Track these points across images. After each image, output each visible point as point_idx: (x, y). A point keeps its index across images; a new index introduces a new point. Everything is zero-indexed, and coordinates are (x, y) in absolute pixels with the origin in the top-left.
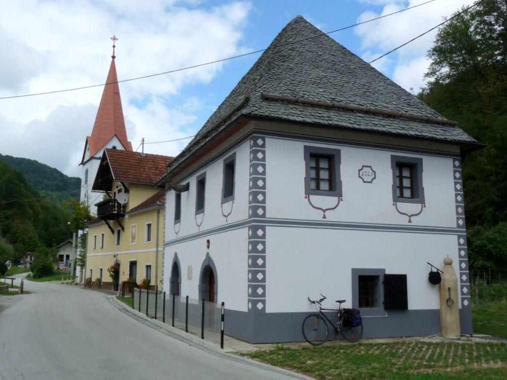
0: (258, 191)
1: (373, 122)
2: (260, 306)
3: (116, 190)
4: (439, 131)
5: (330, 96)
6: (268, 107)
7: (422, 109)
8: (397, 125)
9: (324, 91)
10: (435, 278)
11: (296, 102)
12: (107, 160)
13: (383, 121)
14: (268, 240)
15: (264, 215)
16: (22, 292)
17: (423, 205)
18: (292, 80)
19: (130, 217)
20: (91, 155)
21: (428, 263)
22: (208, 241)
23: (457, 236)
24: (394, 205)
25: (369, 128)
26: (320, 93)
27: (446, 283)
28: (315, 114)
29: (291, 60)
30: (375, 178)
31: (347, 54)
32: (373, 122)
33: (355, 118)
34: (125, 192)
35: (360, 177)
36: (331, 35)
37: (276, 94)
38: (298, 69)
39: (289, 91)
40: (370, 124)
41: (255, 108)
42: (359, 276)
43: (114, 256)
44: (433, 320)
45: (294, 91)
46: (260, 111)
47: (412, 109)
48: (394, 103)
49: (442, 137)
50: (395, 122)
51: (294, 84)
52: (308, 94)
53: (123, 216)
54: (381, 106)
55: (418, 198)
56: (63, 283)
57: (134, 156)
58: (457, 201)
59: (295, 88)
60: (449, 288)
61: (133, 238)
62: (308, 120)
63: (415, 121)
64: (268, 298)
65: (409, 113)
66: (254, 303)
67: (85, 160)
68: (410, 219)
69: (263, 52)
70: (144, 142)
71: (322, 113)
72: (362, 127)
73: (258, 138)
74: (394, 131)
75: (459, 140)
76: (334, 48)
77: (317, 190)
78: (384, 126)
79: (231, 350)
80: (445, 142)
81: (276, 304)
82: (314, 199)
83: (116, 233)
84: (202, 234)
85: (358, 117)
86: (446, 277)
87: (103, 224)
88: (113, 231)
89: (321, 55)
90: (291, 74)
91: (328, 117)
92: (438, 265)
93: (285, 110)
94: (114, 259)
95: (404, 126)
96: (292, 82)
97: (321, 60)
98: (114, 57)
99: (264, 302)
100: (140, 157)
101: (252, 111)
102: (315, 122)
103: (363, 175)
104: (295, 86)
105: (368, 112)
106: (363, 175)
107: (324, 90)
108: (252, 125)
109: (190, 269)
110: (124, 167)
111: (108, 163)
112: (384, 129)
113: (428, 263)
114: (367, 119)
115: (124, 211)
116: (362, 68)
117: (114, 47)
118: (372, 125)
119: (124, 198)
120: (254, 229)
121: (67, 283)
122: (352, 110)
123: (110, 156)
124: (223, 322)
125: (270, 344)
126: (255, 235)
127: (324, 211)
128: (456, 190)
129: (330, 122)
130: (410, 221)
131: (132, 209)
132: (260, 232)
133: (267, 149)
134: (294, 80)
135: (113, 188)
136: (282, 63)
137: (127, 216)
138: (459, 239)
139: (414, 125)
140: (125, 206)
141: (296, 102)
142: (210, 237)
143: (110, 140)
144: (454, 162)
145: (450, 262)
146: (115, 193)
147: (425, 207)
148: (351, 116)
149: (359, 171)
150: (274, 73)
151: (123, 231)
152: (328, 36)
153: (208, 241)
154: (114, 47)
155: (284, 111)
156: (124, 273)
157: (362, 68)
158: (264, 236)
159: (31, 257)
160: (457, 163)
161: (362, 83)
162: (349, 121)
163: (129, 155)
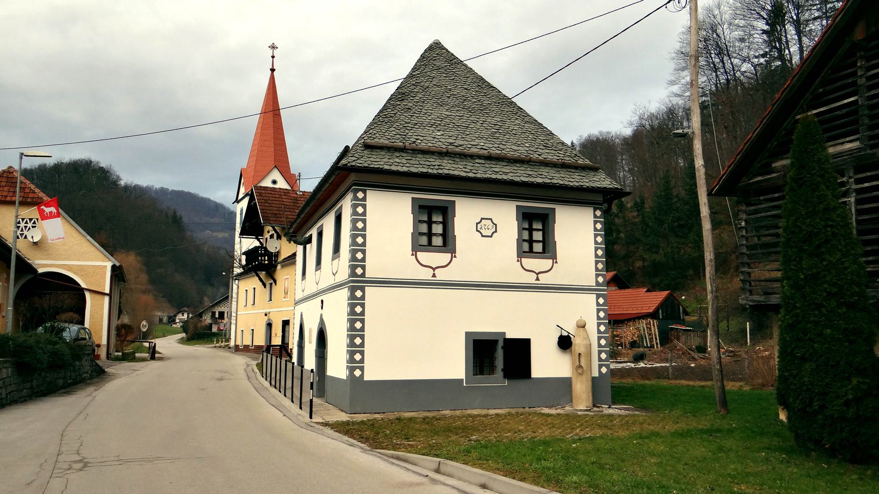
0: (359, 248)
1: (493, 169)
2: (357, 373)
3: (267, 236)
4: (575, 176)
5: (447, 141)
6: (370, 156)
7: (561, 150)
8: (523, 172)
9: (442, 135)
10: (565, 343)
11: (403, 150)
12: (255, 200)
13: (506, 167)
14: (367, 302)
15: (363, 275)
16: (153, 358)
17: (555, 260)
18: (406, 123)
19: (283, 267)
20: (245, 191)
21: (558, 326)
22: (322, 301)
23: (595, 295)
24: (518, 261)
25: (487, 176)
26: (437, 137)
27: (577, 348)
28: (424, 163)
29: (411, 98)
30: (496, 231)
31: (484, 86)
32: (493, 169)
33: (473, 165)
34: (277, 239)
35: (496, 225)
36: (470, 64)
37: (384, 141)
38: (417, 108)
39: (399, 137)
40: (489, 172)
41: (354, 158)
42: (474, 341)
43: (266, 315)
44: (562, 387)
45: (405, 135)
46: (359, 161)
47: (548, 151)
48: (526, 145)
49: (577, 184)
50: (522, 168)
51: (408, 128)
52: (422, 138)
53: (276, 267)
54: (509, 150)
55: (549, 253)
56: (215, 347)
57: (289, 195)
58: (596, 256)
59: (407, 131)
60: (580, 354)
61: (286, 293)
62: (414, 170)
63: (549, 166)
64: (366, 365)
65: (543, 156)
66: (351, 370)
67: (240, 197)
68: (537, 277)
69: (398, 84)
70: (301, 178)
71: (434, 160)
72: (478, 176)
73: (357, 191)
74: (517, 179)
75: (598, 187)
76: (469, 80)
77: (429, 246)
78: (506, 173)
79: (321, 420)
80: (580, 189)
81: (373, 372)
82: (423, 256)
83: (268, 286)
84: (306, 299)
85: (476, 165)
86: (578, 343)
87: (254, 276)
88: (264, 285)
89: (450, 90)
90: (407, 115)
91: (438, 166)
92: (570, 328)
93: (389, 159)
94: (266, 318)
95: (531, 173)
96: (406, 125)
97: (449, 95)
98: (273, 70)
99: (362, 369)
100: (295, 196)
101: (349, 162)
102: (421, 172)
103: (481, 228)
104: (408, 130)
105: (489, 158)
106: (481, 228)
107: (443, 133)
108: (353, 177)
109: (310, 330)
110: (275, 209)
111: (256, 202)
112: (505, 177)
113: (558, 326)
114: (488, 166)
115: (276, 261)
116: (499, 103)
117: (273, 57)
118: (491, 173)
119: (276, 245)
120: (353, 290)
121: (220, 347)
122: (472, 157)
123: (260, 195)
124: (311, 391)
125: (369, 414)
126: (352, 297)
127: (434, 269)
128: (596, 242)
129: (440, 171)
130: (538, 279)
131: (285, 259)
132: (359, 294)
133: (369, 203)
134: (409, 123)
135: (264, 234)
136: (398, 103)
137: (279, 267)
138: (597, 299)
139: (545, 171)
140: (277, 254)
141: (403, 150)
142: (324, 297)
143: (269, 172)
144: (595, 211)
145: (583, 325)
146: (267, 238)
147: (556, 262)
148: (468, 163)
149: (477, 224)
150: (385, 115)
151: (276, 284)
152: (466, 66)
153: (322, 301)
154: (273, 57)
155: (388, 160)
156: (276, 334)
157: (499, 103)
158: (363, 298)
159: (188, 314)
160: (598, 213)
161: (493, 122)
162: (464, 170)
163: (283, 194)
